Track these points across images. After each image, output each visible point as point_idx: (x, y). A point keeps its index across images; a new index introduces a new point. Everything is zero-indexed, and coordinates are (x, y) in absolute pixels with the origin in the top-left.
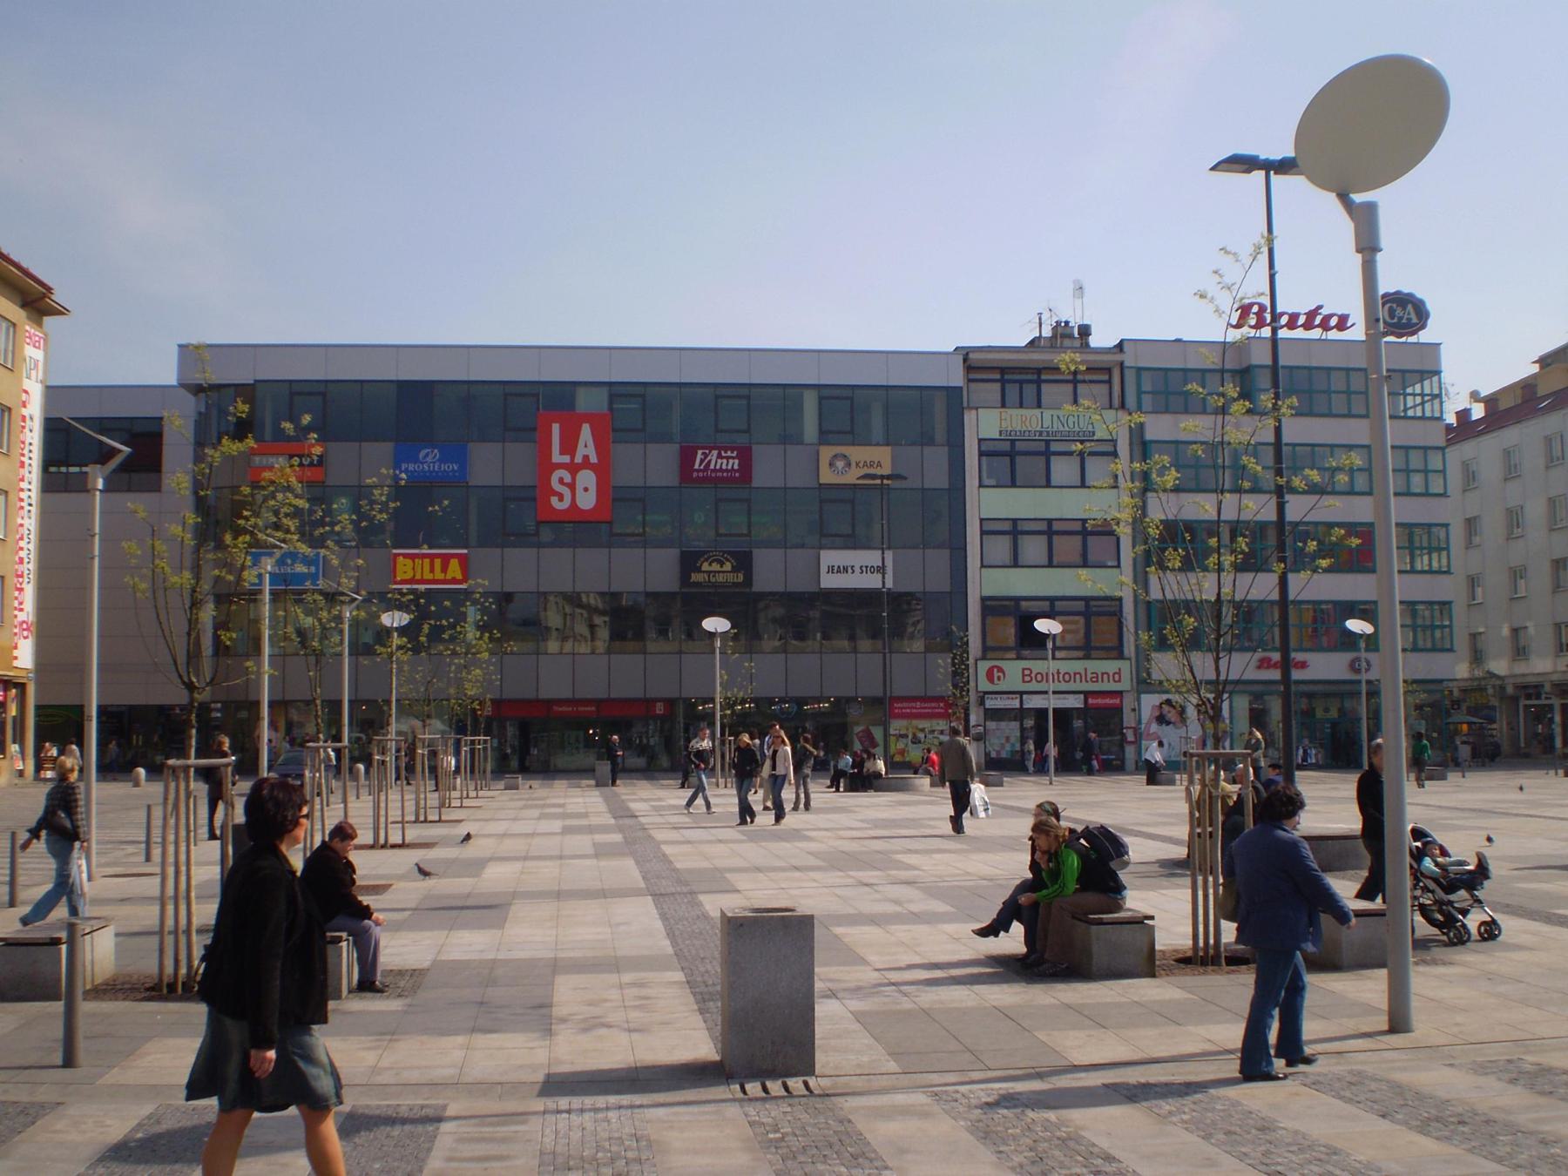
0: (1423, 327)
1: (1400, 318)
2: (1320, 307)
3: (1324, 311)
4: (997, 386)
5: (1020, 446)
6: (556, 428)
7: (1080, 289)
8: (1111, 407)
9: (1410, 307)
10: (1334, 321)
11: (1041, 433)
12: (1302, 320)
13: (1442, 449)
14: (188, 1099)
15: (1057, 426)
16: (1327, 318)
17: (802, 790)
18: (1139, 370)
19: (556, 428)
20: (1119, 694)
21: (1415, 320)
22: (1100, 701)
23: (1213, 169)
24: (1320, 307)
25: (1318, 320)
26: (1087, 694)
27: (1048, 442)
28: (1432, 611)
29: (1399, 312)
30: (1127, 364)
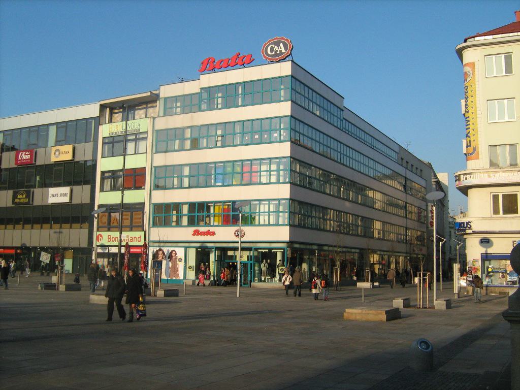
9: (281, 45)
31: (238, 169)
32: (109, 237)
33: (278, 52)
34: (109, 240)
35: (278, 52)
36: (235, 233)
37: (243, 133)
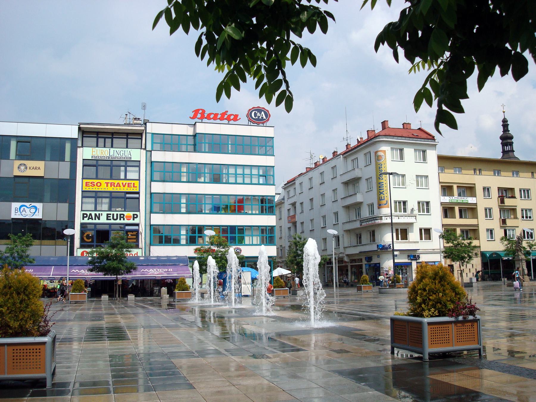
1: (259, 117)
3: (228, 114)
4: (96, 139)
5: (100, 163)
7: (144, 107)
9: (263, 113)
10: (232, 117)
12: (219, 116)
14: (393, 320)
15: (116, 155)
16: (209, 115)
17: (184, 354)
21: (265, 118)
23: (417, 110)
25: (226, 117)
28: (399, 307)
29: (258, 114)
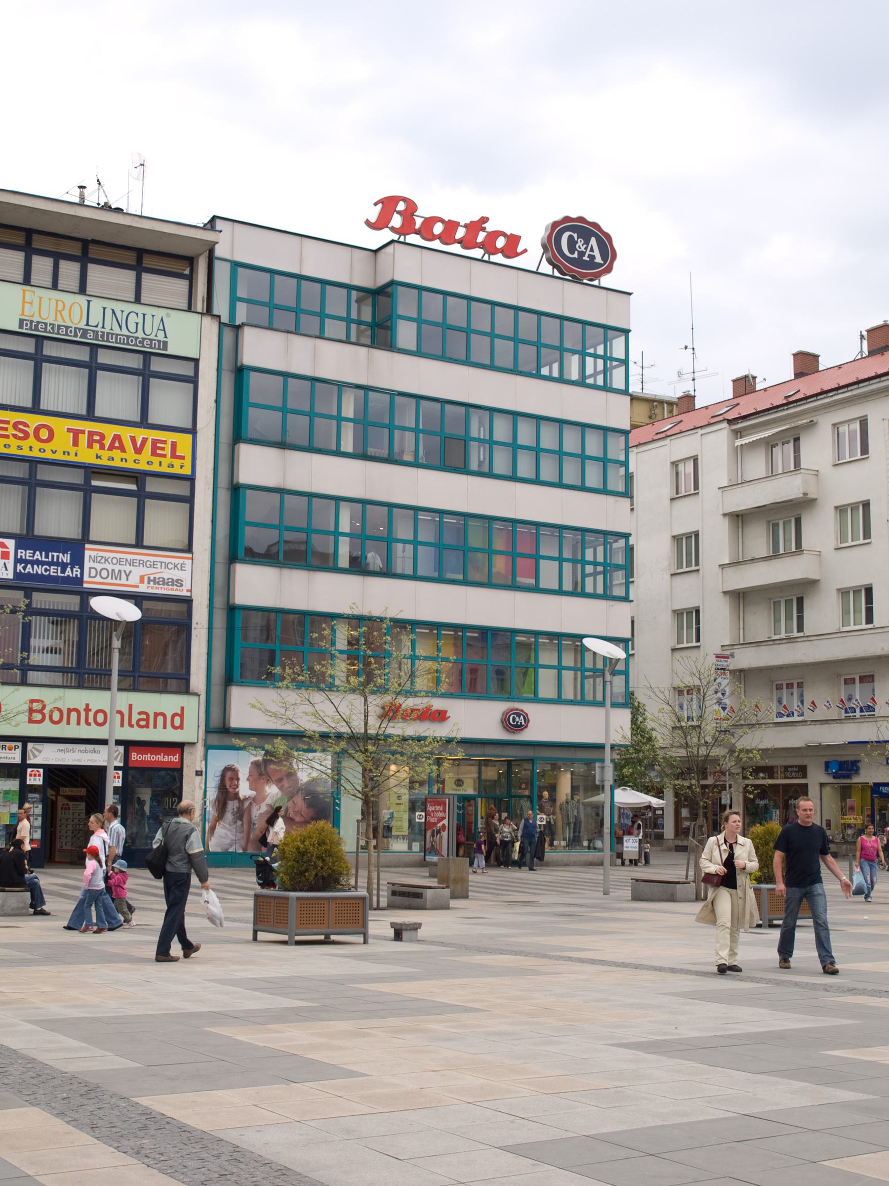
0: (609, 270)
1: (581, 254)
2: (484, 220)
3: (490, 227)
6: (476, 635)
8: (190, 309)
9: (593, 241)
11: (85, 333)
12: (460, 233)
13: (625, 433)
15: (110, 325)
18: (236, 265)
19: (476, 635)
20: (179, 747)
21: (598, 260)
22: (148, 757)
24: (484, 220)
25: (481, 237)
26: (128, 745)
27: (94, 348)
29: (580, 243)
30: (219, 252)
31: (499, 544)
32: (36, 706)
33: (586, 258)
34: (38, 717)
35: (586, 258)
36: (527, 720)
37: (359, 537)
